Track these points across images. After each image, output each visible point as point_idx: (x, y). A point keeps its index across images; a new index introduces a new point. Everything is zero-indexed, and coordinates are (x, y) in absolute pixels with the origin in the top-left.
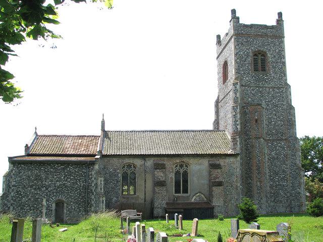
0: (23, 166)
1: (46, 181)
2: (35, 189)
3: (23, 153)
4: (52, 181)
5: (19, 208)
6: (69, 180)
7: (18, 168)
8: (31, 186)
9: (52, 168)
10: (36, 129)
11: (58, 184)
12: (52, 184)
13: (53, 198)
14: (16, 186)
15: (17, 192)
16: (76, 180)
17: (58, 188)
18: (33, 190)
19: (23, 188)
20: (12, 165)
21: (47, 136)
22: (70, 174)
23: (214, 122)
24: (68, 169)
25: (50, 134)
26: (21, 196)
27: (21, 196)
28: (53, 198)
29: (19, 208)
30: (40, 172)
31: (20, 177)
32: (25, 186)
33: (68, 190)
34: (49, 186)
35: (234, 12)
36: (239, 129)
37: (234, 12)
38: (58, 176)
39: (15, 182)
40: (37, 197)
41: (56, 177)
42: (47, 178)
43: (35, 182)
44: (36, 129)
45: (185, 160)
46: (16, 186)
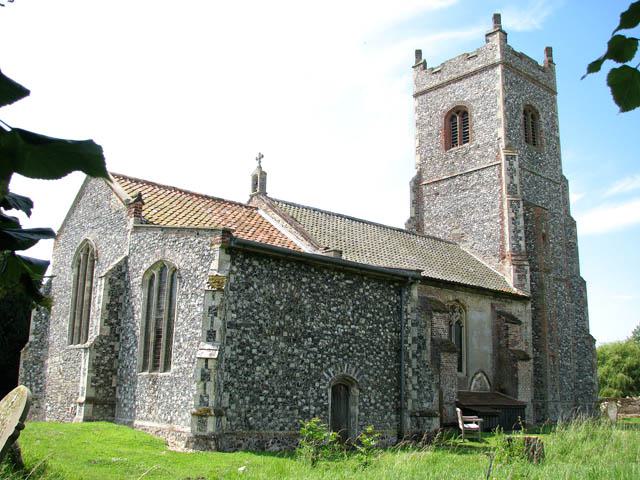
0: (255, 263)
1: (312, 320)
2: (288, 340)
3: (397, 212)
4: (325, 320)
5: (247, 398)
6: (363, 321)
7: (243, 268)
8: (278, 332)
9: (326, 282)
10: (583, 77)
11: (340, 329)
12: (327, 329)
13: (330, 370)
14: (237, 327)
15: (242, 346)
16: (378, 322)
17: (341, 342)
18: (282, 345)
19: (257, 337)
20: (228, 257)
21: (192, 194)
22: (365, 305)
23: (409, 222)
24: (361, 290)
25: (63, 219)
26: (250, 361)
27: (250, 361)
28: (330, 370)
29: (247, 398)
30: (298, 291)
31: (250, 298)
32: (260, 326)
33: (361, 351)
34: (320, 335)
35: (419, 53)
36: (523, 248)
37: (419, 53)
38: (342, 307)
39: (236, 311)
40: (292, 365)
41: (334, 309)
42: (315, 310)
43: (288, 318)
44: (583, 77)
45: (461, 296)
46: (237, 327)
